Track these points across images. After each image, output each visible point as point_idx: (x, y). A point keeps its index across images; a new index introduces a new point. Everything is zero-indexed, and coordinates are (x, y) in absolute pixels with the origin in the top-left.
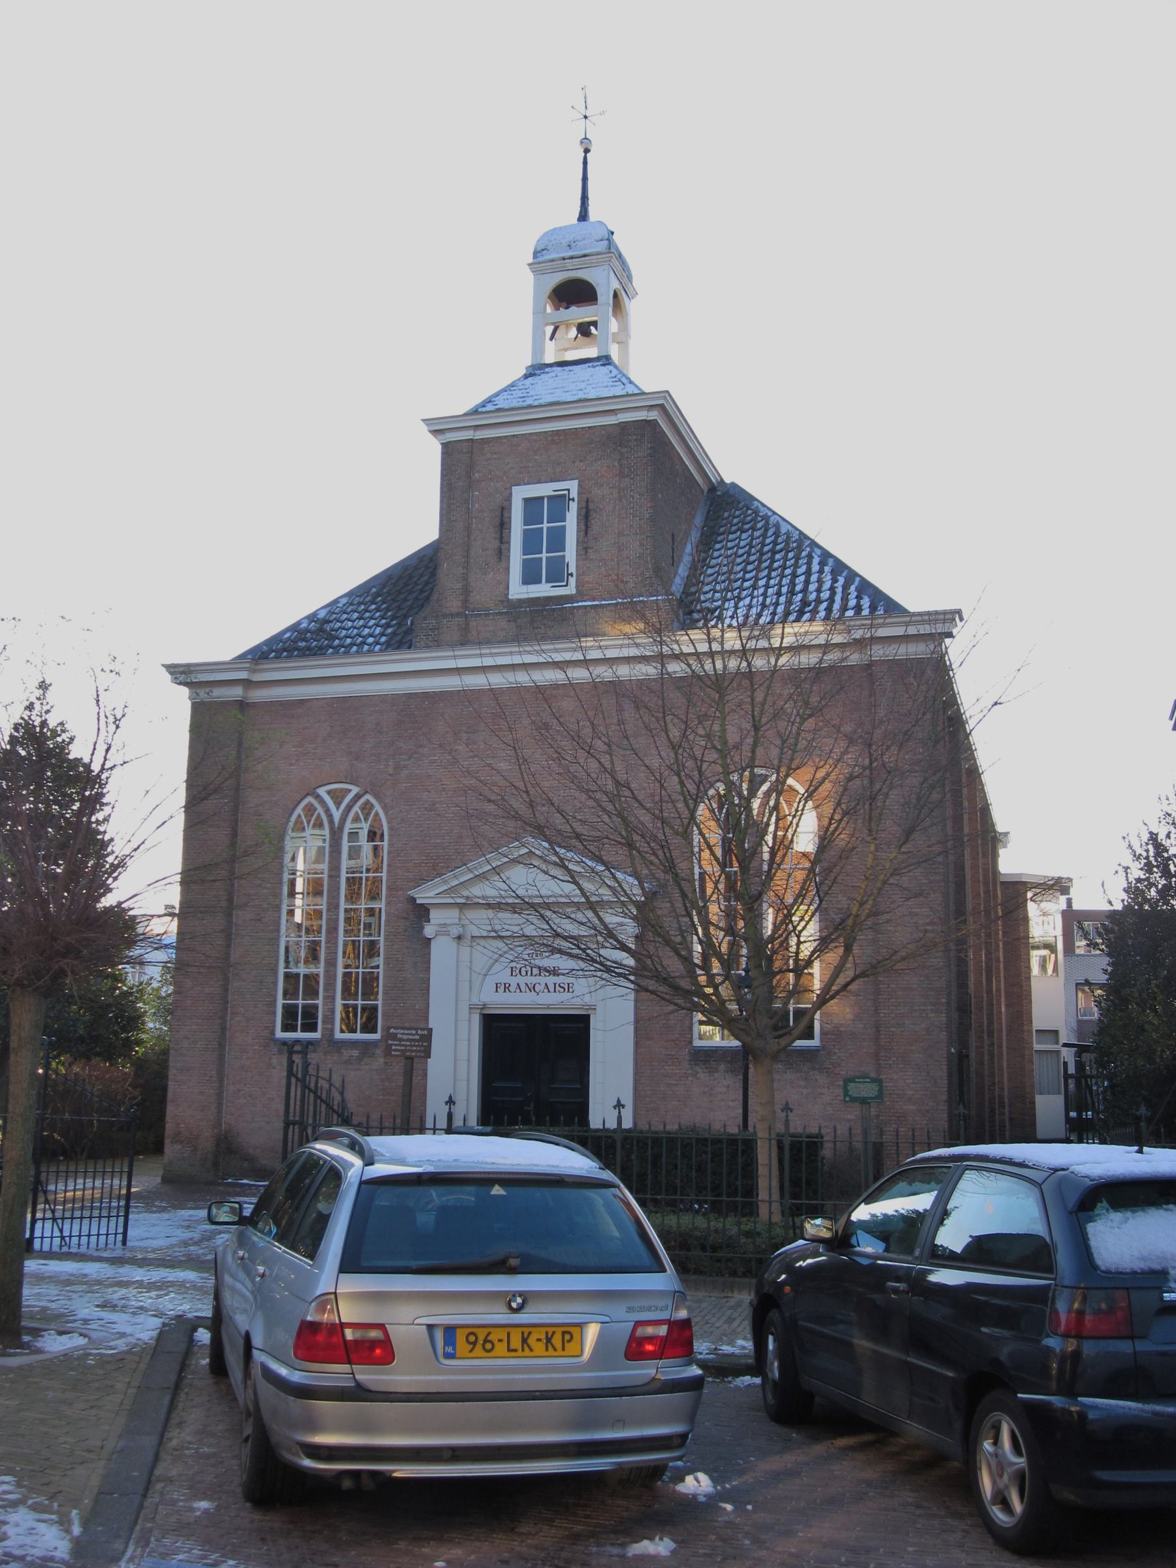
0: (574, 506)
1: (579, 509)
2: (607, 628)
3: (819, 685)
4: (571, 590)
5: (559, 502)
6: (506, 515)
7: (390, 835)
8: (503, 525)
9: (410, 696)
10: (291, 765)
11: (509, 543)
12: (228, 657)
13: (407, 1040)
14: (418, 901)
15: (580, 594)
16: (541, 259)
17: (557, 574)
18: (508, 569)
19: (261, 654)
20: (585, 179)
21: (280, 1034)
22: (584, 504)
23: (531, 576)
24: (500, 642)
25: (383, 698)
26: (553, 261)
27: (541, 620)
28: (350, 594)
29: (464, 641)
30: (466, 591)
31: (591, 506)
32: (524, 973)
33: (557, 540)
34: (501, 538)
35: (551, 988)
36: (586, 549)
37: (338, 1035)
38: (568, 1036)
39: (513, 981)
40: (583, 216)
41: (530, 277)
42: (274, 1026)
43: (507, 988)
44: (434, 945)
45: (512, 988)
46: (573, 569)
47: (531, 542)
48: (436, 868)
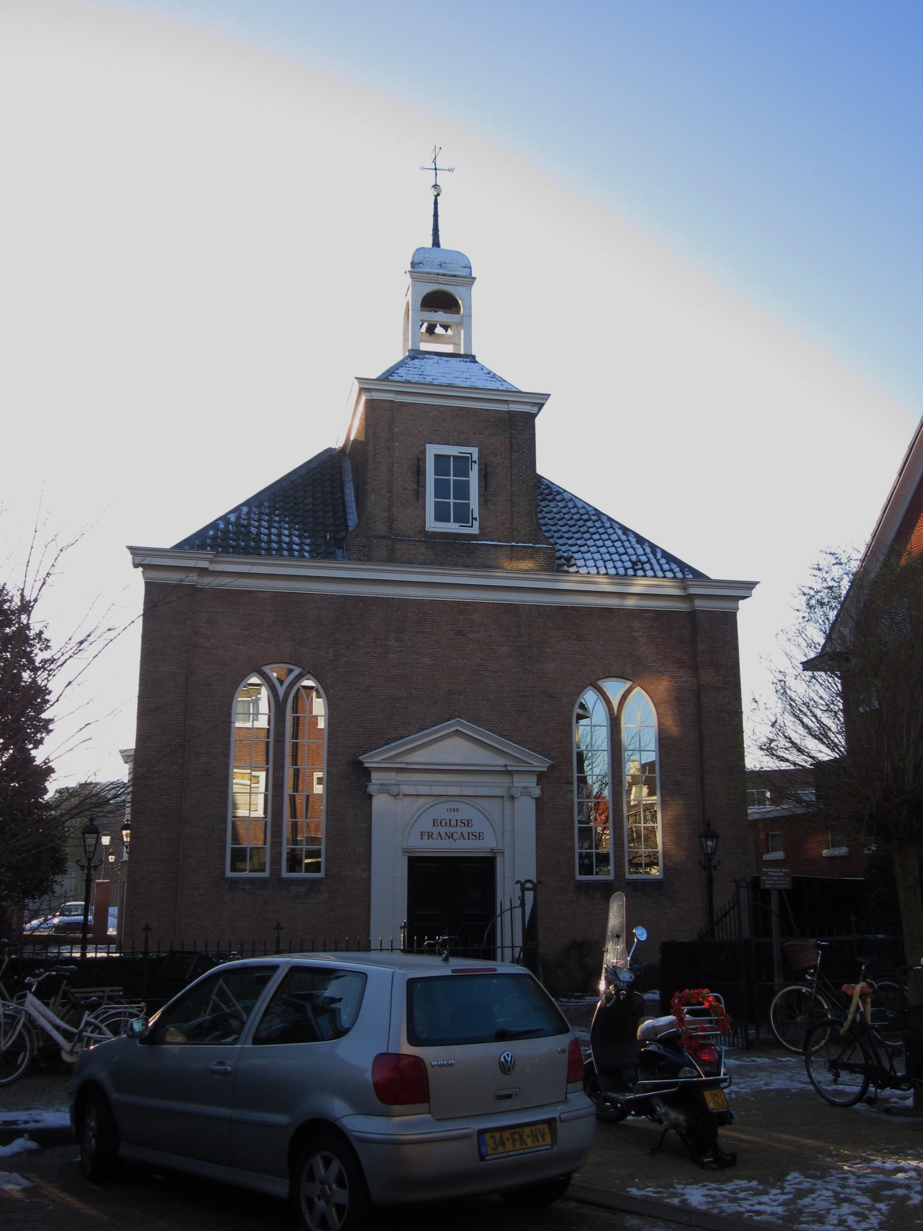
0: (476, 467)
1: (480, 470)
2: (506, 564)
3: (658, 621)
4: (475, 530)
5: (463, 463)
6: (421, 465)
7: (571, 717)
8: (419, 473)
9: (346, 598)
10: (238, 644)
11: (425, 487)
12: (168, 545)
13: (776, 876)
14: (366, 765)
15: (482, 535)
16: (418, 270)
17: (463, 516)
18: (424, 507)
19: (198, 542)
20: (436, 216)
21: (229, 874)
22: (483, 467)
23: (441, 516)
24: (420, 564)
25: (323, 597)
26: (429, 273)
27: (451, 551)
28: (247, 503)
29: (391, 559)
30: (391, 520)
31: (489, 469)
32: (443, 824)
33: (462, 491)
34: (418, 483)
35: (466, 836)
36: (486, 501)
37: (285, 874)
38: (479, 871)
39: (436, 831)
40: (436, 243)
41: (408, 280)
42: (224, 868)
43: (430, 836)
44: (375, 801)
45: (435, 836)
46: (476, 515)
47: (441, 489)
48: (381, 737)
